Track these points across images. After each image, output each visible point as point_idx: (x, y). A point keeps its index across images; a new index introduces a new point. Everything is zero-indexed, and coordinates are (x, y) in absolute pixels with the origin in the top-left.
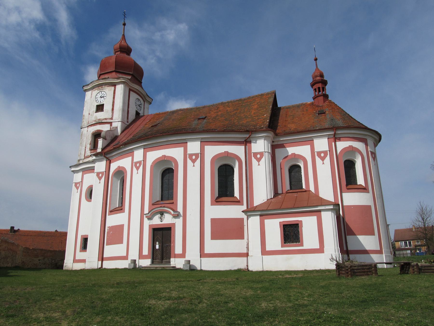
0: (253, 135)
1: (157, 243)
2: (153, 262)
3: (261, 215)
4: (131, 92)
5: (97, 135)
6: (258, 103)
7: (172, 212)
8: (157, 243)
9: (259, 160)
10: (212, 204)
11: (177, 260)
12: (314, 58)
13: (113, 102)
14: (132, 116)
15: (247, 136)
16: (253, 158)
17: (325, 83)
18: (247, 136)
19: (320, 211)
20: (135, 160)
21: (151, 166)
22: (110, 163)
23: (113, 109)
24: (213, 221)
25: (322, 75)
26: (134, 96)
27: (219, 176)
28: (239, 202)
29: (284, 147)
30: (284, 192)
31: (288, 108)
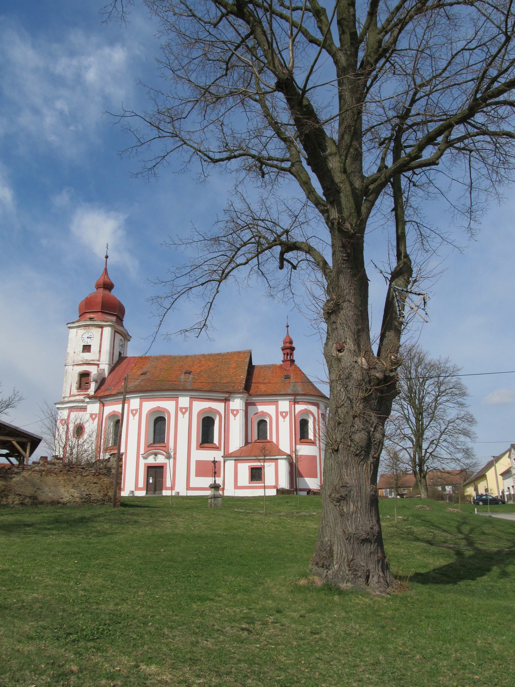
0: (232, 395)
1: (151, 478)
2: (147, 493)
3: (235, 460)
4: (116, 334)
5: (84, 376)
6: (236, 361)
7: (165, 453)
8: (151, 478)
9: (235, 415)
10: (197, 449)
11: (167, 491)
12: (286, 324)
13: (101, 344)
14: (116, 358)
15: (227, 396)
16: (230, 414)
17: (293, 349)
18: (227, 396)
19: (277, 459)
20: (131, 408)
21: (147, 415)
22: (104, 406)
23: (100, 351)
24: (198, 462)
25: (291, 342)
26: (118, 337)
27: (203, 426)
28: (218, 448)
29: (256, 405)
30: (253, 441)
31: (262, 367)
